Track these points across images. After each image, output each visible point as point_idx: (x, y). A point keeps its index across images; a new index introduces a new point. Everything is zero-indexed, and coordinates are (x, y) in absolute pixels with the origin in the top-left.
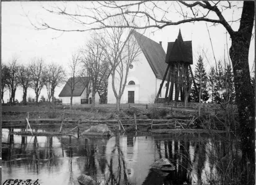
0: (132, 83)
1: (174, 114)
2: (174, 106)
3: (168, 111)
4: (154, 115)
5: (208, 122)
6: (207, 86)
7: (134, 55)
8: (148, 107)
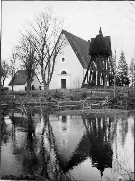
0: (64, 73)
1: (93, 96)
3: (88, 94)
6: (128, 74)
7: (59, 48)
8: (72, 91)
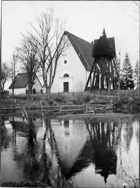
1: (96, 99)
2: (99, 93)
4: (124, 103)
5: (125, 106)
8: (75, 94)
